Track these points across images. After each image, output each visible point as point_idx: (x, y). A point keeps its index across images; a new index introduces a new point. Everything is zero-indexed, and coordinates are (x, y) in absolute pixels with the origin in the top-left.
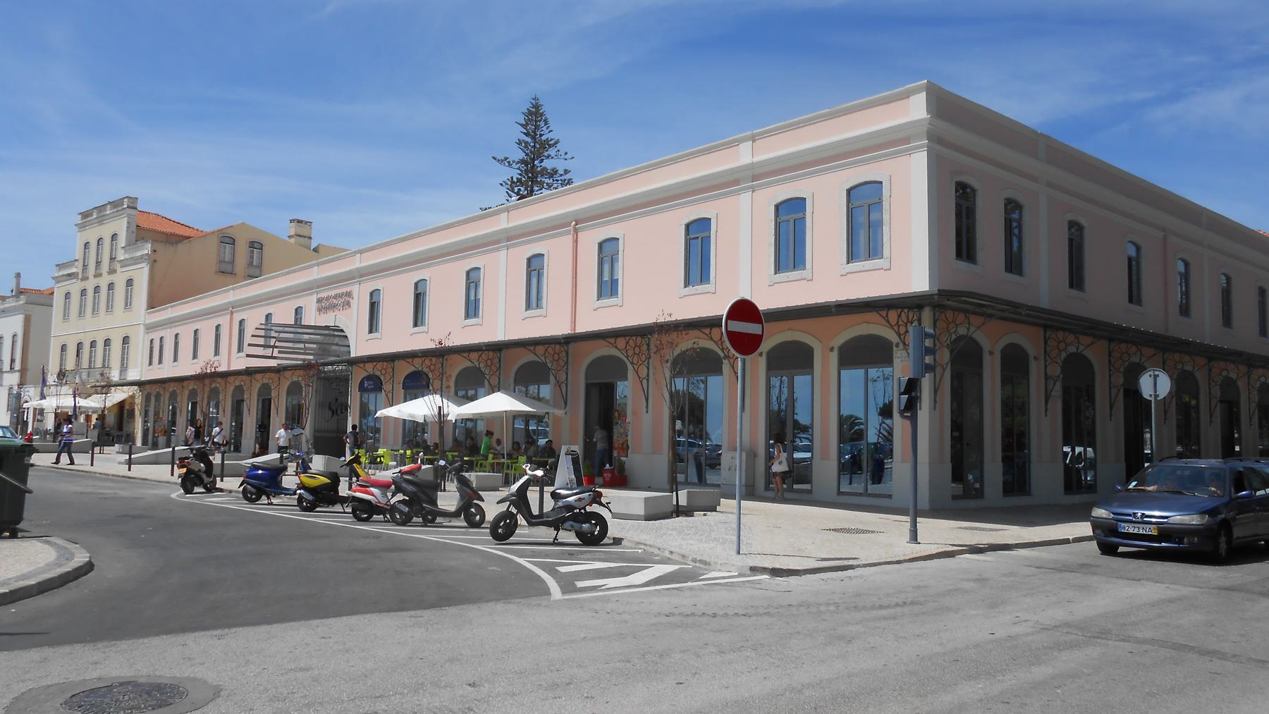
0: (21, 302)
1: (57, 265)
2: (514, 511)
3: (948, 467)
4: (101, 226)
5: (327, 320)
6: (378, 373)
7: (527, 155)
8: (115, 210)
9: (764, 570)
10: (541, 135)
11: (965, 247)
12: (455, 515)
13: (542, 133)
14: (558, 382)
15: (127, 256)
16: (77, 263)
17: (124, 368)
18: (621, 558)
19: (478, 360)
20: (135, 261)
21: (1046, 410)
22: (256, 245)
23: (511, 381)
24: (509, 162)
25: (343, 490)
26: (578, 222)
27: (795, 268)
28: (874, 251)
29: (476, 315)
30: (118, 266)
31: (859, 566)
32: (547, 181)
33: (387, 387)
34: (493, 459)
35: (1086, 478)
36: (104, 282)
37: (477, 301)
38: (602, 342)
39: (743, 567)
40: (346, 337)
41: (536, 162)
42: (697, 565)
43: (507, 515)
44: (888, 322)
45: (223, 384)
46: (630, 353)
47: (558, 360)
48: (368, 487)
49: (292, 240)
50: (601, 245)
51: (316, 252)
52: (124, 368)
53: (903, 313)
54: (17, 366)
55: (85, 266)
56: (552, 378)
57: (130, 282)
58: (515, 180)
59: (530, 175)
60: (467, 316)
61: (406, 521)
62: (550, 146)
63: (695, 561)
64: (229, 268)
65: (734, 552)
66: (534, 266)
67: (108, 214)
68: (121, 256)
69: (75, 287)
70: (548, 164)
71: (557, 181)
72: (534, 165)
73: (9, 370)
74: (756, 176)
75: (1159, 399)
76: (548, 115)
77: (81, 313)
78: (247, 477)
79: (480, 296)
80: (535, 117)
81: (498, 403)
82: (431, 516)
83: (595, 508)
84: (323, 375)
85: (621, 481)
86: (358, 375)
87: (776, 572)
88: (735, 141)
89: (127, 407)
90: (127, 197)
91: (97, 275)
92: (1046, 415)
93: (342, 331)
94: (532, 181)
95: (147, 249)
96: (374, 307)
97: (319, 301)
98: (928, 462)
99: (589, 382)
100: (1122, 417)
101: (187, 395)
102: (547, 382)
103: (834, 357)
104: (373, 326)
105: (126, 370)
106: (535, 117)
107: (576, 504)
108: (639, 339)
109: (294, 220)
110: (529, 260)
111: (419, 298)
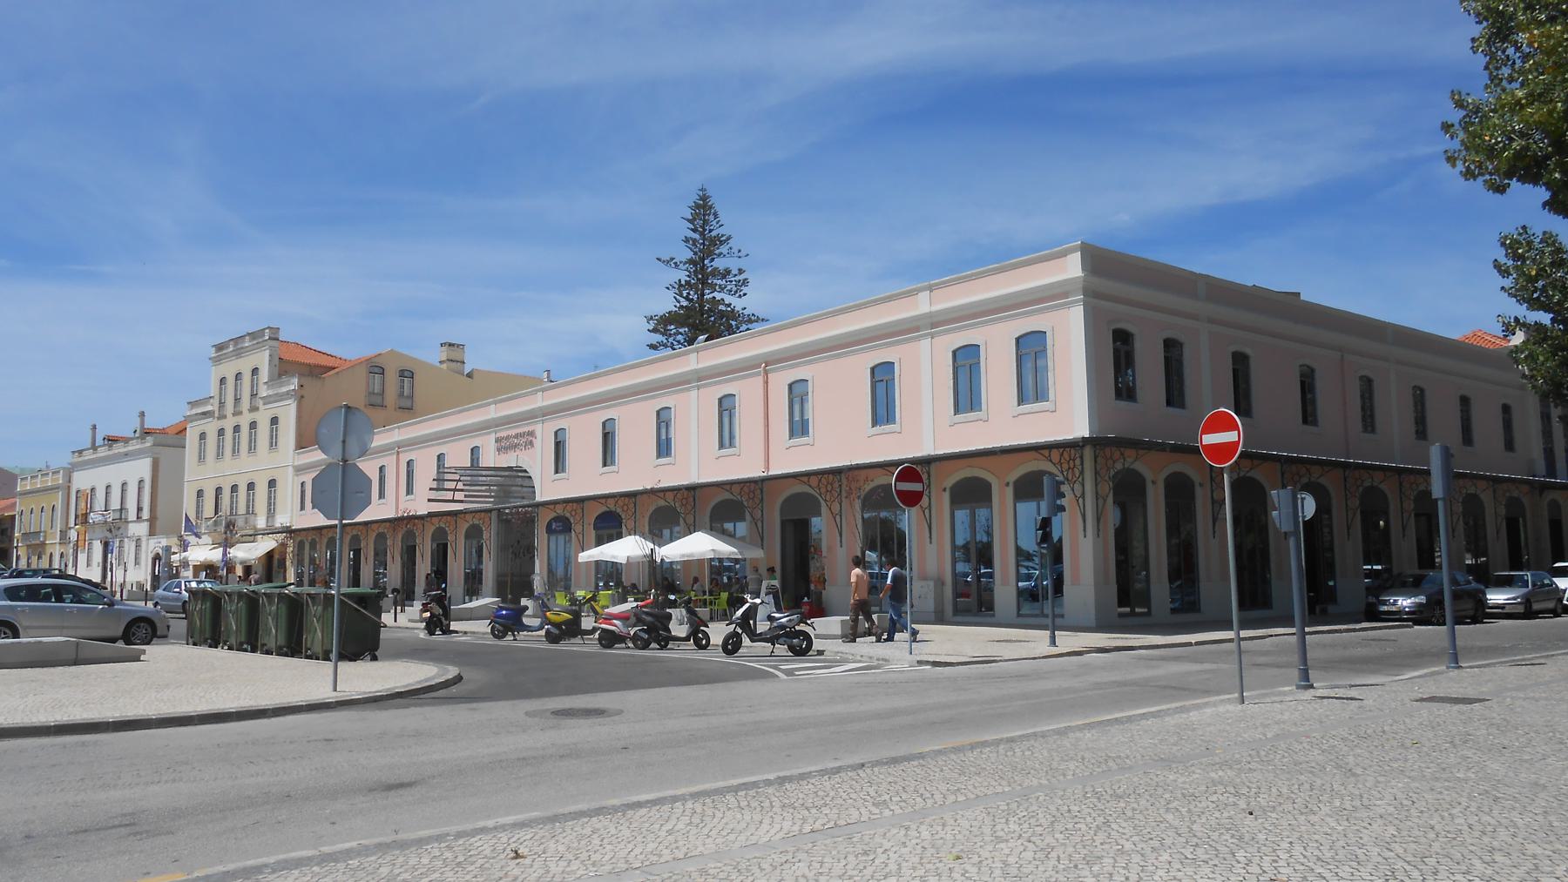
0: (148, 444)
1: (189, 403)
2: (740, 631)
3: (1114, 588)
4: (239, 360)
5: (508, 460)
6: (568, 515)
7: (695, 253)
8: (255, 342)
9: (927, 663)
10: (711, 231)
11: (1125, 392)
12: (687, 639)
13: (712, 228)
14: (754, 519)
15: (271, 392)
16: (211, 400)
17: (271, 513)
18: (824, 661)
20: (280, 397)
21: (1214, 532)
22: (406, 374)
23: (707, 519)
24: (675, 263)
25: (587, 623)
26: (768, 363)
27: (972, 410)
28: (1040, 394)
29: (668, 454)
30: (260, 403)
31: (1001, 661)
32: (719, 282)
33: (578, 528)
36: (244, 420)
37: (668, 440)
39: (913, 661)
40: (530, 477)
41: (706, 262)
42: (880, 662)
43: (735, 635)
45: (364, 532)
48: (610, 619)
49: (444, 366)
50: (790, 386)
51: (469, 377)
52: (271, 513)
54: (146, 514)
55: (222, 404)
56: (748, 516)
57: (274, 421)
58: (683, 282)
59: (700, 276)
60: (659, 455)
61: (646, 646)
62: (722, 243)
63: (878, 660)
64: (378, 400)
65: (908, 654)
66: (726, 406)
67: (247, 347)
68: (264, 392)
69: (211, 427)
70: (720, 264)
71: (732, 281)
72: (704, 265)
73: (135, 519)
74: (934, 323)
75: (1306, 519)
76: (717, 207)
77: (219, 454)
78: (495, 617)
79: (672, 435)
80: (703, 210)
81: (699, 545)
82: (665, 640)
83: (802, 627)
84: (505, 517)
85: (820, 611)
86: (544, 518)
87: (935, 664)
88: (915, 290)
89: (276, 557)
90: (269, 328)
91: (237, 413)
93: (525, 471)
94: (703, 284)
95: (293, 384)
96: (559, 447)
97: (497, 440)
98: (1093, 583)
99: (784, 518)
100: (1360, 536)
101: (325, 544)
102: (743, 519)
103: (1010, 491)
104: (559, 464)
105: (274, 516)
106: (703, 210)
107: (787, 624)
109: (445, 344)
110: (720, 400)
111: (608, 438)
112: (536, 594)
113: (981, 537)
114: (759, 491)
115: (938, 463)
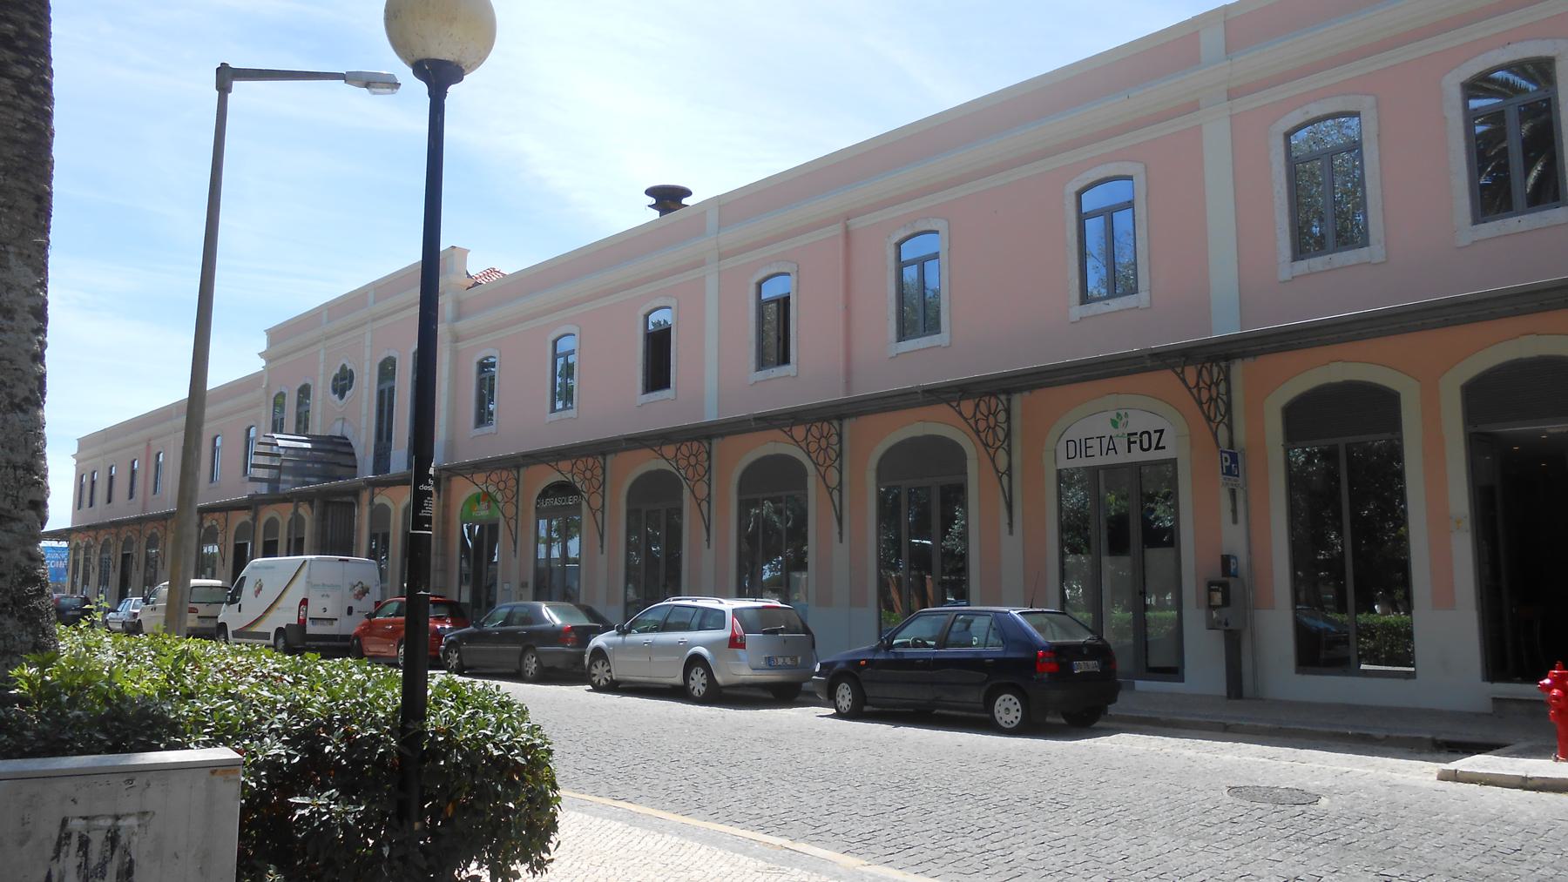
19: (806, 438)
27: (1554, 201)
35: (931, 646)
44: (792, 437)
46: (813, 447)
47: (825, 450)
53: (982, 402)
93: (350, 445)
112: (1358, 616)
114: (600, 471)
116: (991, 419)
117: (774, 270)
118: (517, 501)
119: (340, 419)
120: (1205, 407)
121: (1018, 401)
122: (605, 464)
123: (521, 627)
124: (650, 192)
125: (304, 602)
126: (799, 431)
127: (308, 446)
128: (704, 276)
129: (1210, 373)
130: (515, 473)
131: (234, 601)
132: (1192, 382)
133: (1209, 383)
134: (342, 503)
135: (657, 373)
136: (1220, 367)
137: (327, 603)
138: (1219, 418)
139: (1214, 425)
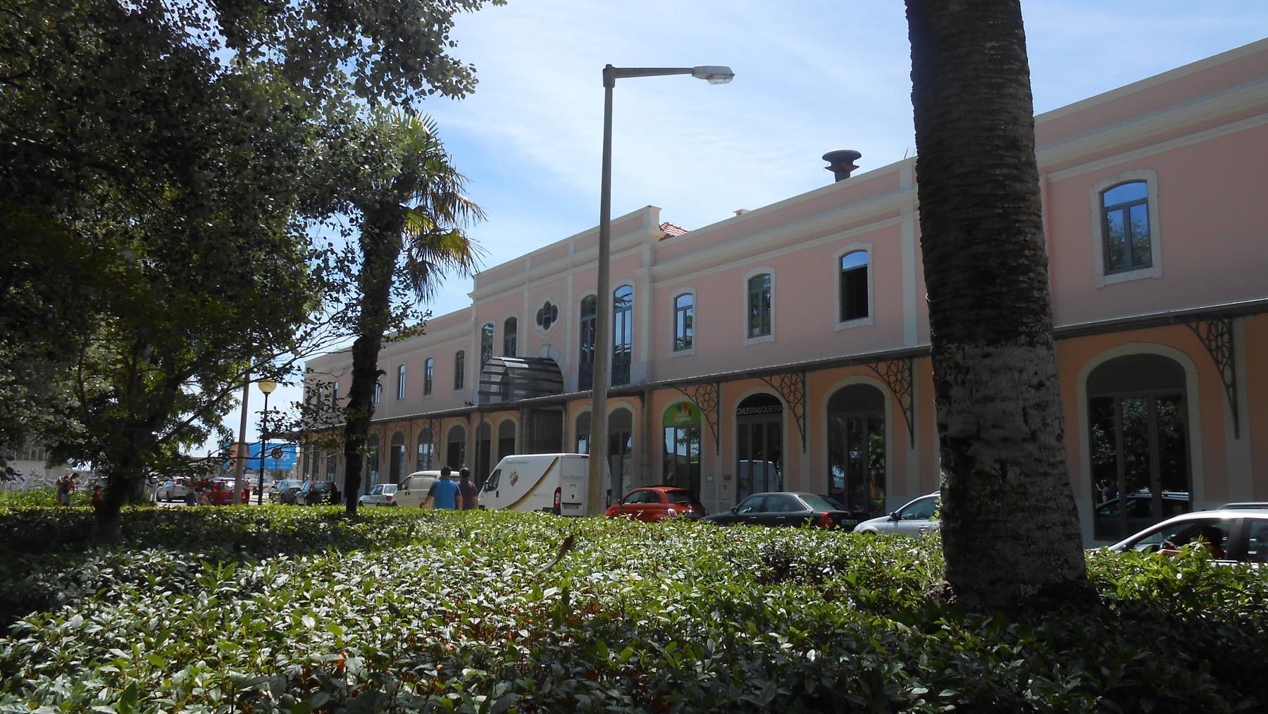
34: (1108, 500)
38: (758, 380)
44: (878, 372)
53: (893, 365)
92: (913, 447)
93: (556, 365)
108: (794, 377)
113: (615, 458)
115: (1250, 318)
116: (899, 375)
117: (852, 248)
118: (718, 409)
119: (545, 345)
120: (893, 386)
121: (808, 375)
122: (911, 366)
123: (778, 513)
124: (826, 157)
125: (558, 490)
126: (882, 367)
127: (526, 366)
128: (900, 224)
129: (1217, 326)
130: (801, 375)
131: (491, 489)
132: (1204, 335)
133: (1215, 334)
134: (551, 411)
135: (428, 388)
136: (1224, 323)
137: (574, 491)
138: (1225, 360)
139: (1221, 366)
